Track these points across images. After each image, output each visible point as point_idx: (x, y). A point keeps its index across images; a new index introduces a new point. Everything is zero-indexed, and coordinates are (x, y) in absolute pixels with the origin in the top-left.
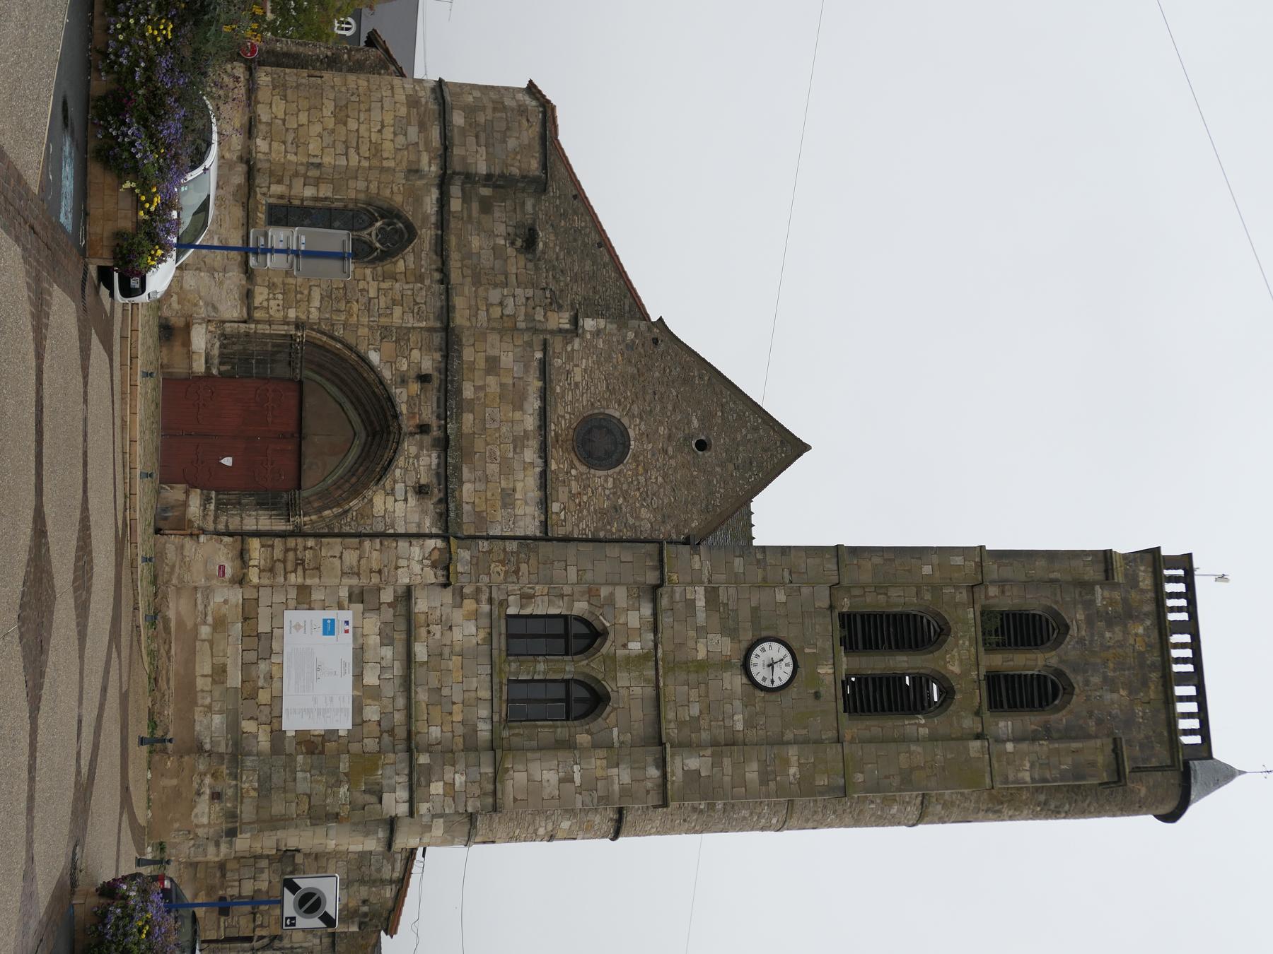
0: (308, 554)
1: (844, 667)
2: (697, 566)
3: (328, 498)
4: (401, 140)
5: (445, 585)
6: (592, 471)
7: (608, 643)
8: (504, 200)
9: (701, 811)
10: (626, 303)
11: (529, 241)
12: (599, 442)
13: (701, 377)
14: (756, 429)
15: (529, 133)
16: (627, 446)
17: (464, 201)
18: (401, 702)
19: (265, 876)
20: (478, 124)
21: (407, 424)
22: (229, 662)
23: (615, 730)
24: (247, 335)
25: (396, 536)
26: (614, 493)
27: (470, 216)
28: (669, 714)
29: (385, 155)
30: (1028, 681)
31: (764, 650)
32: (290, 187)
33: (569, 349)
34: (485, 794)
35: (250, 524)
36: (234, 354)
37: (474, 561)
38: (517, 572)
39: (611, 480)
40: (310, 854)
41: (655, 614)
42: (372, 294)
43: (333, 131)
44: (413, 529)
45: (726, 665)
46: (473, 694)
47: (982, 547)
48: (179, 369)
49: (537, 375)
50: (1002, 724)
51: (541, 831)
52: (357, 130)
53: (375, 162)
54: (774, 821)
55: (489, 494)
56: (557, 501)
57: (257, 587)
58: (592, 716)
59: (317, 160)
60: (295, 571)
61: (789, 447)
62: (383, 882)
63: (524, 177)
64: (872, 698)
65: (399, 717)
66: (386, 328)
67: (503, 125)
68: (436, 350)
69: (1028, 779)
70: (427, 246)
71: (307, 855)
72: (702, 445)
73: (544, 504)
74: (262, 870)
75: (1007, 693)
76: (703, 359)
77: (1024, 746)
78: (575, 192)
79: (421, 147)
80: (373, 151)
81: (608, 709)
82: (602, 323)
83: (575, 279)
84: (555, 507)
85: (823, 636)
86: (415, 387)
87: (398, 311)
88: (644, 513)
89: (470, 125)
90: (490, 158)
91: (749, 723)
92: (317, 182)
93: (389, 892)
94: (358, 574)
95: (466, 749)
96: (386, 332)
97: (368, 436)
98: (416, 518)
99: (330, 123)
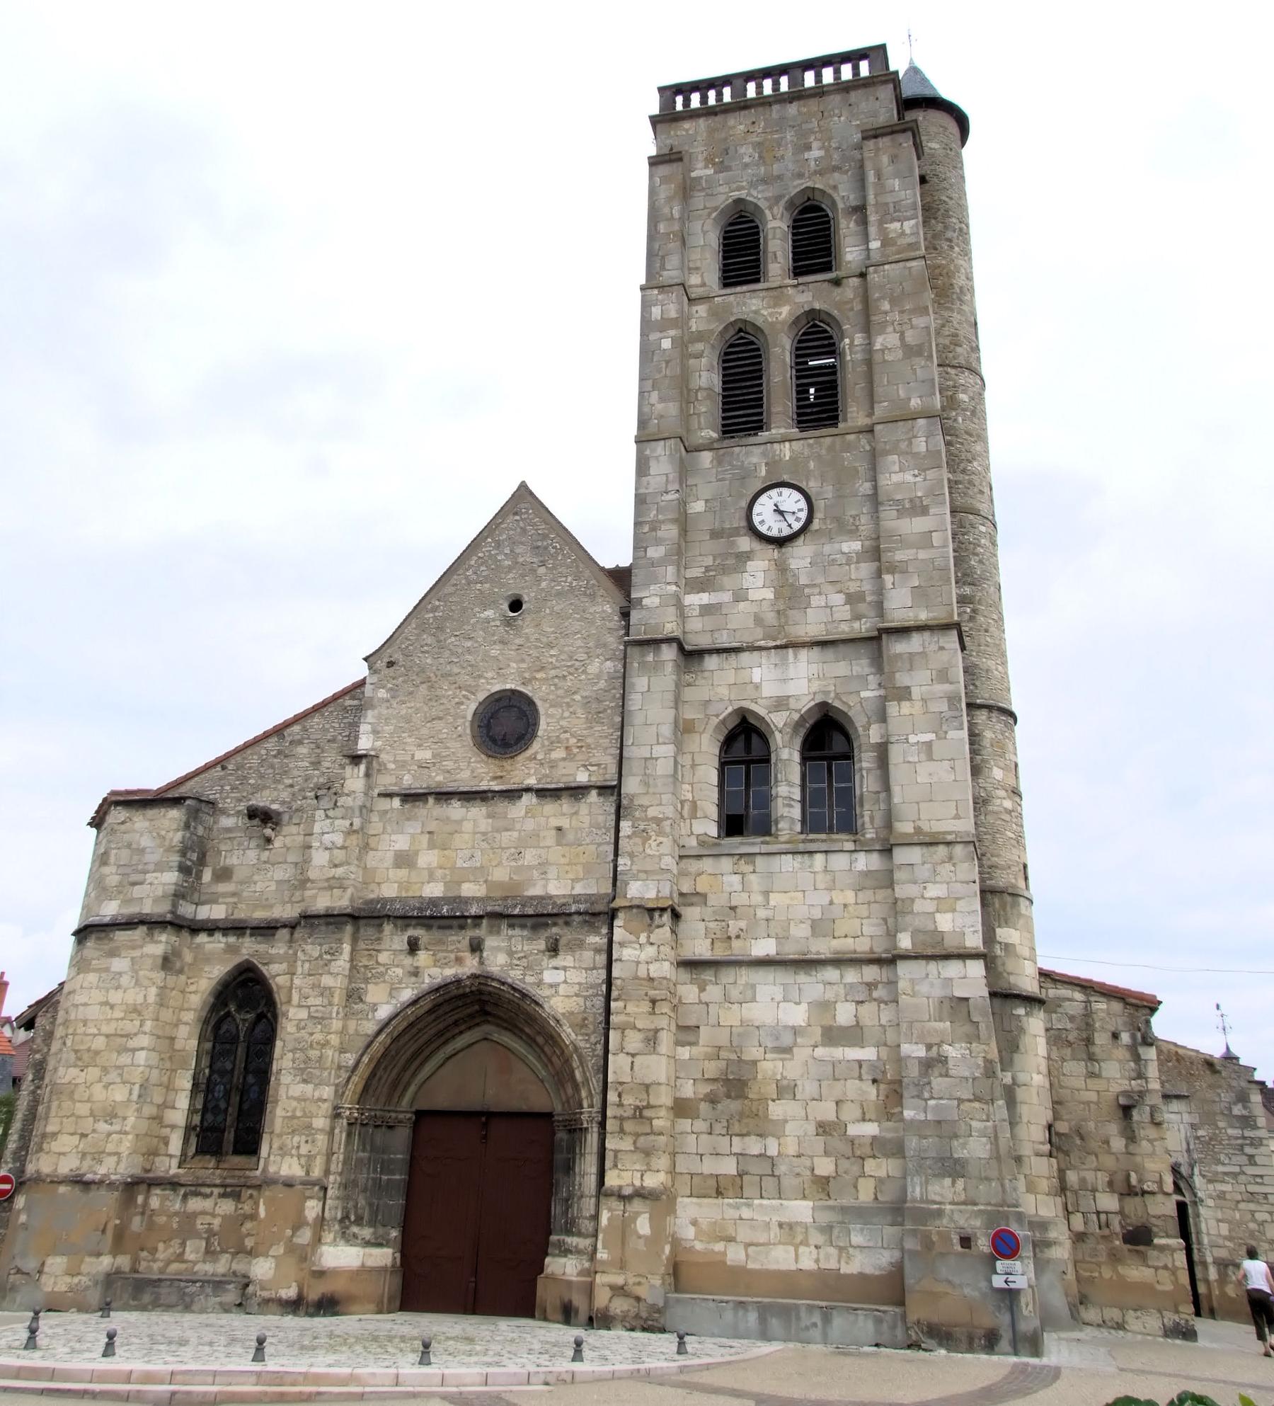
0: (628, 1100)
1: (782, 431)
2: (657, 600)
3: (563, 1076)
4: (125, 980)
5: (676, 916)
6: (540, 733)
7: (753, 707)
8: (219, 852)
9: (974, 611)
10: (350, 700)
11: (262, 817)
12: (506, 724)
13: (435, 609)
14: (498, 545)
15: (140, 821)
16: (513, 691)
17: (215, 902)
18: (831, 974)
19: (1089, 1176)
20: (121, 884)
21: (470, 966)
22: (775, 1219)
23: (864, 694)
24: (344, 1186)
25: (609, 982)
26: (568, 705)
27: (234, 894)
28: (845, 630)
29: (140, 1000)
30: (805, 263)
31: (762, 522)
32: (173, 1127)
33: (393, 766)
34: (951, 858)
35: (590, 1182)
36: (371, 1205)
37: (643, 876)
38: (658, 821)
39: (551, 711)
40: (1055, 1111)
41: (719, 651)
42: (303, 1014)
43: (105, 1070)
44: (602, 959)
45: (782, 567)
46: (820, 877)
47: (643, 288)
48: (389, 1285)
49: (421, 804)
50: (849, 257)
51: (1008, 804)
52: (107, 1036)
53: (149, 1013)
54: (983, 529)
55: (563, 861)
56: (574, 775)
57: (672, 1172)
58: (851, 732)
59: (136, 1088)
60: (650, 1119)
61: (523, 505)
62: (1088, 1014)
63: (187, 826)
64: (820, 408)
65: (852, 976)
66: (349, 997)
67: (125, 853)
68: (381, 931)
69: (913, 222)
70: (262, 947)
71: (1057, 1116)
72: (516, 605)
73: (577, 792)
74: (1083, 1181)
75: (814, 245)
76: (415, 608)
77: (873, 230)
78: (219, 768)
79: (137, 953)
80: (134, 1015)
81: (837, 704)
82: (364, 728)
83: (316, 764)
84: (582, 778)
85: (752, 456)
86: (423, 957)
87: (327, 981)
88: (593, 668)
89: (120, 892)
90: (160, 867)
91: (853, 533)
92: (169, 1087)
93: (1101, 1005)
94: (657, 1031)
95: (891, 885)
96: (353, 996)
97: (489, 1022)
98: (588, 955)
99: (93, 1073)
